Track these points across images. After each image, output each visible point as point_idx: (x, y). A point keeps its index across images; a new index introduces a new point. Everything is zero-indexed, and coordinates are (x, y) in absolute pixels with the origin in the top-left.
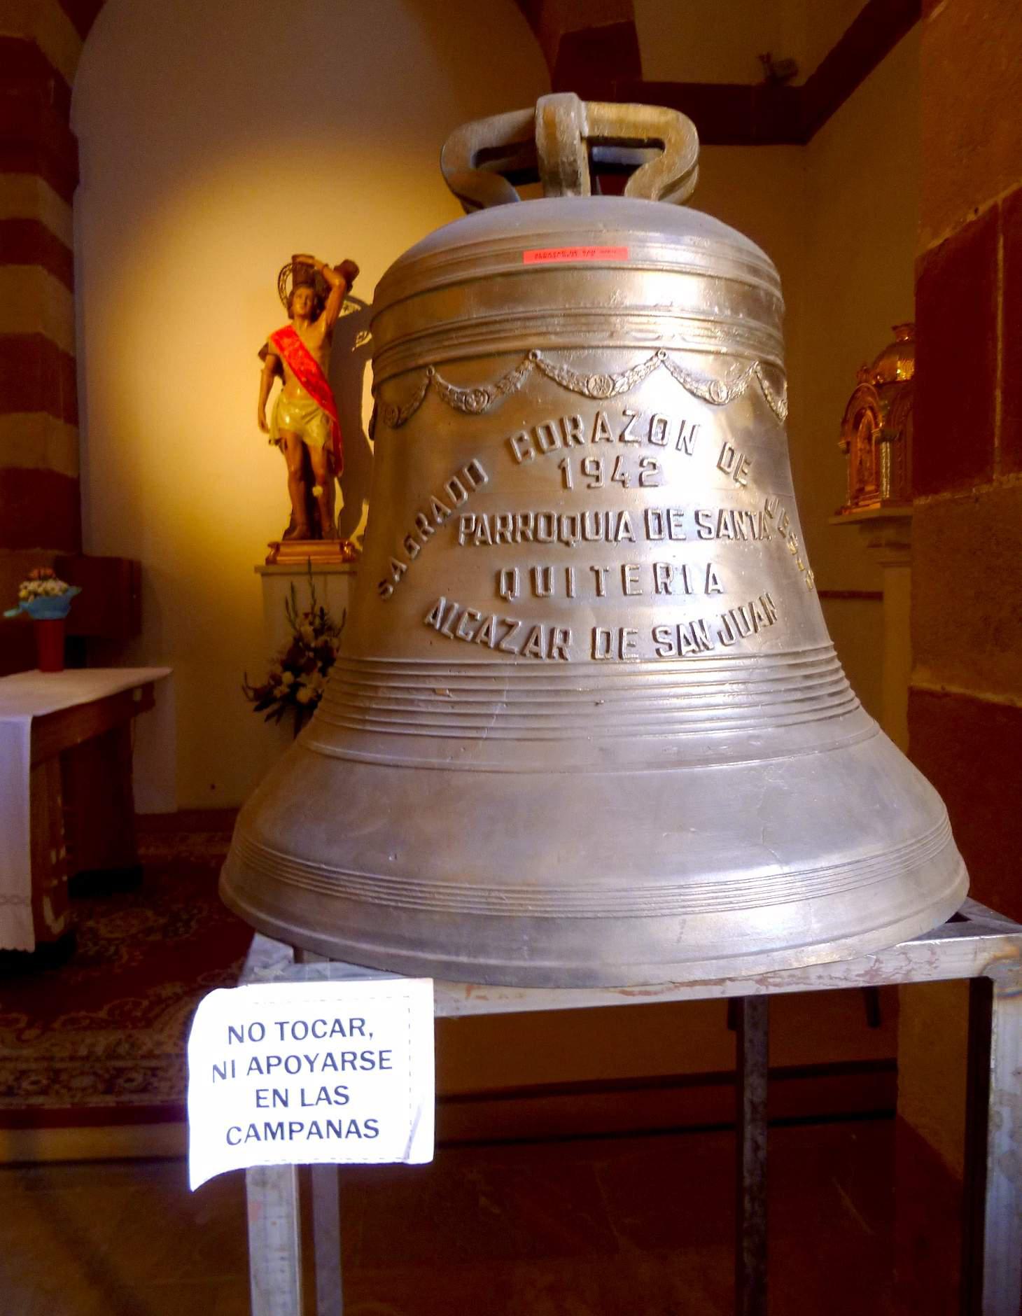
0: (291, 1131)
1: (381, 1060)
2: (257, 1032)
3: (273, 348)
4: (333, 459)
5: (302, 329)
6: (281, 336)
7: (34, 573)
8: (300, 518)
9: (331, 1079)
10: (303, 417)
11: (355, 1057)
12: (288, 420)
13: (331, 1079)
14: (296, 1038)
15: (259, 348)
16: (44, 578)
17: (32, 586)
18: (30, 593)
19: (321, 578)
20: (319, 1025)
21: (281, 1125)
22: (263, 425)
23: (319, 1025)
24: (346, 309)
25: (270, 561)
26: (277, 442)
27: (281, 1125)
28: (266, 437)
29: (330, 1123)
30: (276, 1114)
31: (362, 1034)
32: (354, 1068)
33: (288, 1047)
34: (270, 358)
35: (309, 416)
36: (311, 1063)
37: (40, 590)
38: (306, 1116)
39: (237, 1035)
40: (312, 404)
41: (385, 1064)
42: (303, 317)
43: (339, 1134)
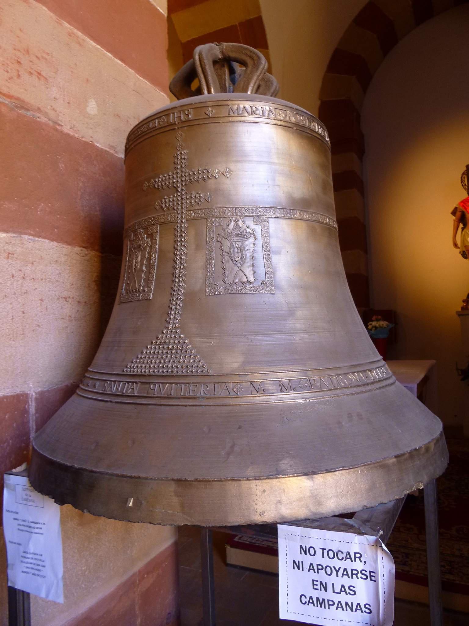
0: (329, 605)
1: (371, 576)
2: (312, 552)
3: (461, 208)
7: (374, 318)
9: (347, 581)
11: (358, 573)
13: (347, 581)
14: (330, 558)
15: (452, 209)
16: (377, 320)
17: (374, 323)
18: (373, 327)
20: (340, 553)
21: (324, 600)
22: (456, 245)
23: (340, 553)
27: (324, 600)
28: (458, 250)
29: (347, 604)
30: (322, 595)
31: (361, 562)
32: (358, 578)
33: (326, 562)
34: (458, 214)
36: (337, 572)
37: (377, 325)
38: (336, 598)
39: (303, 550)
41: (373, 578)
43: (352, 610)
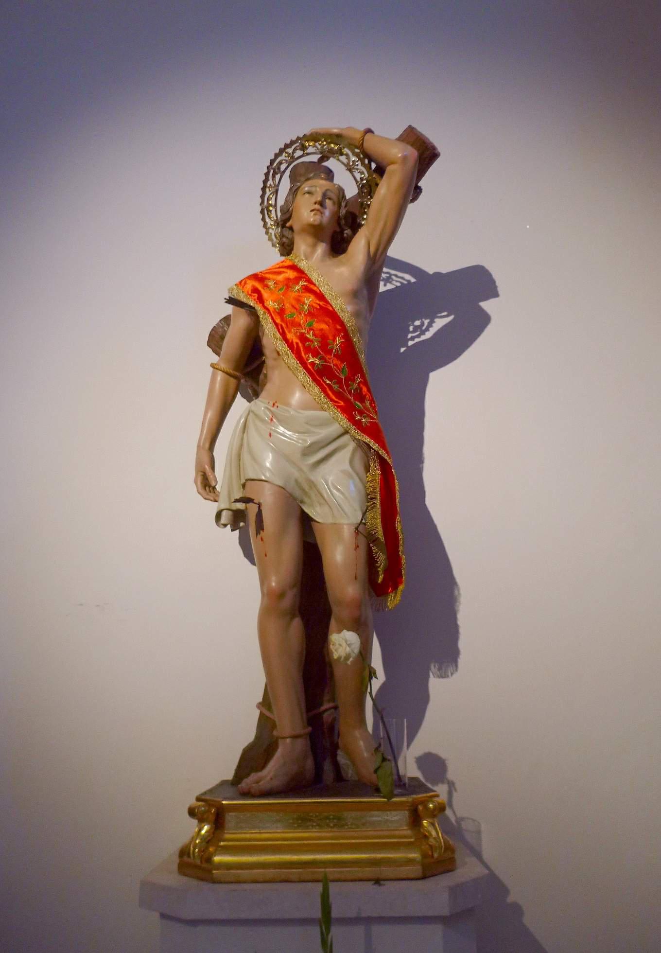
4: (382, 559)
5: (311, 257)
6: (249, 298)
8: (289, 721)
10: (308, 451)
12: (268, 461)
19: (359, 931)
22: (207, 485)
24: (388, 280)
25: (194, 864)
26: (238, 518)
28: (212, 508)
35: (319, 452)
40: (331, 421)
42: (316, 231)
